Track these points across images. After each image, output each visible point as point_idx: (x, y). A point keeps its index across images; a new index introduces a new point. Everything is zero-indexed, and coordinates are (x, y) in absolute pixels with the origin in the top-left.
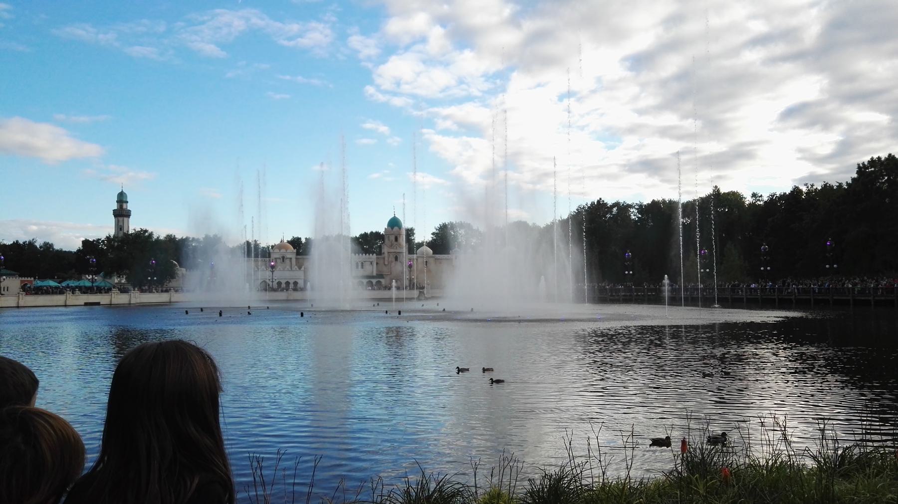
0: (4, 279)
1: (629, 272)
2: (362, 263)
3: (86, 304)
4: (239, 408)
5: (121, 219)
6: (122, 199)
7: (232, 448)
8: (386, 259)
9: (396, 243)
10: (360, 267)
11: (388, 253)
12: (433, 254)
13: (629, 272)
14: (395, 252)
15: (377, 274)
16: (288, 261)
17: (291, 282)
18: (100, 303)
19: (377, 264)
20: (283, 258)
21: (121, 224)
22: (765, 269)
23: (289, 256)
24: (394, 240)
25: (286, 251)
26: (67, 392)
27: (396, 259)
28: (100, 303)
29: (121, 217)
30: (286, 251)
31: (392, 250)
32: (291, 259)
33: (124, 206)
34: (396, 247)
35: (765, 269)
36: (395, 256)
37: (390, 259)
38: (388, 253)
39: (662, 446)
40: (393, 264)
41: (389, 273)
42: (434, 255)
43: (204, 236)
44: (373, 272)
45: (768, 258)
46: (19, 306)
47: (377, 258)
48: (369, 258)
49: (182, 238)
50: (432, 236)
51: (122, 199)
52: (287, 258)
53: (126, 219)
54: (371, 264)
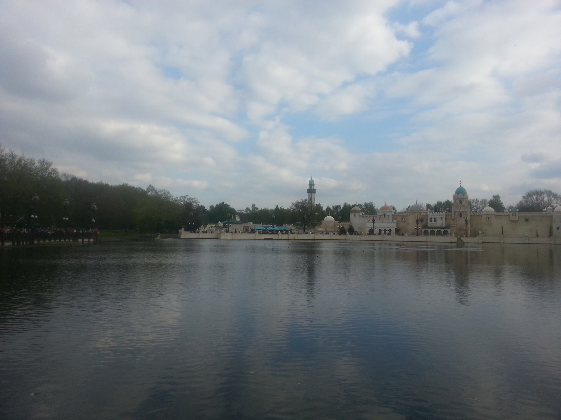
0: (231, 225)
3: (266, 239)
5: (310, 194)
7: (9, 324)
8: (453, 216)
11: (454, 211)
14: (459, 211)
15: (445, 226)
16: (387, 217)
17: (388, 229)
18: (272, 238)
19: (446, 219)
20: (384, 215)
21: (310, 196)
22: (191, 224)
23: (387, 214)
24: (459, 202)
25: (386, 210)
28: (272, 238)
29: (313, 193)
30: (386, 210)
32: (389, 215)
33: (312, 187)
34: (461, 208)
36: (460, 213)
38: (454, 211)
41: (456, 225)
46: (315, 239)
49: (361, 204)
52: (386, 215)
53: (313, 194)
54: (441, 219)
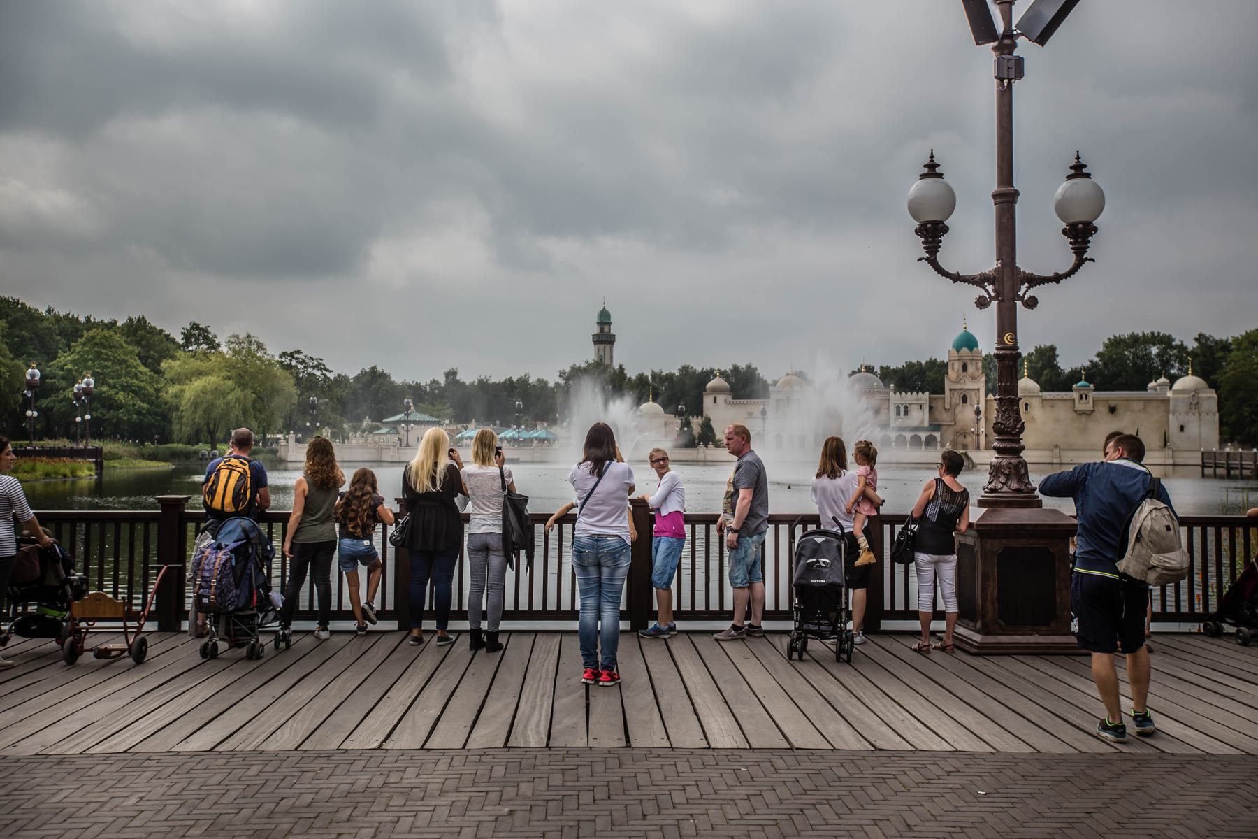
1: (83, 419)
2: (906, 407)
4: (226, 486)
6: (604, 319)
8: (947, 400)
9: (964, 374)
10: (902, 413)
11: (951, 390)
12: (1041, 391)
13: (83, 419)
26: (286, 804)
27: (965, 400)
31: (958, 386)
35: (83, 417)
37: (954, 401)
38: (951, 390)
39: (50, 396)
40: (959, 409)
41: (953, 423)
42: (1040, 394)
43: (731, 367)
44: (923, 421)
45: (79, 419)
47: (930, 398)
48: (917, 400)
50: (1096, 359)
51: (604, 319)
53: (608, 347)
